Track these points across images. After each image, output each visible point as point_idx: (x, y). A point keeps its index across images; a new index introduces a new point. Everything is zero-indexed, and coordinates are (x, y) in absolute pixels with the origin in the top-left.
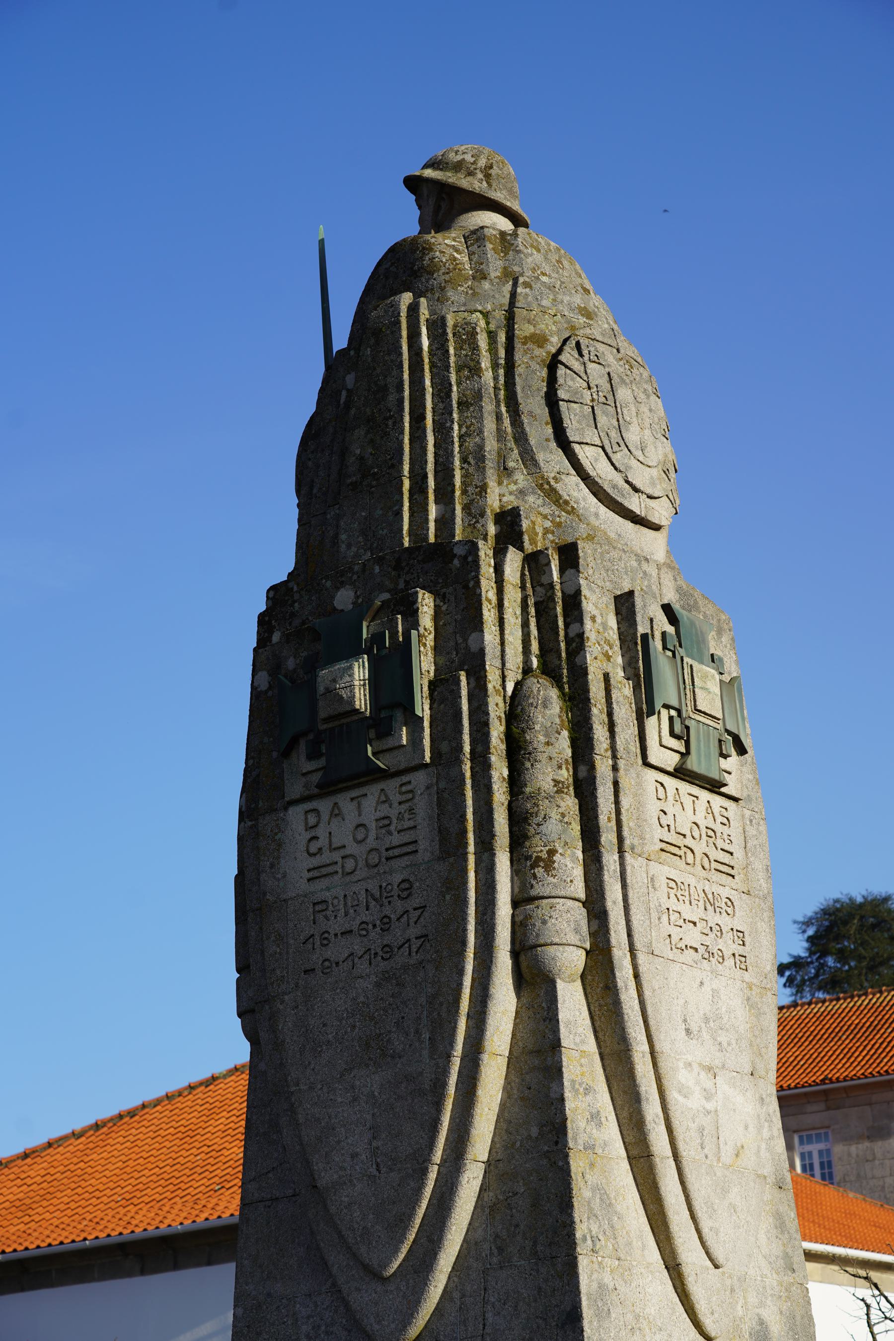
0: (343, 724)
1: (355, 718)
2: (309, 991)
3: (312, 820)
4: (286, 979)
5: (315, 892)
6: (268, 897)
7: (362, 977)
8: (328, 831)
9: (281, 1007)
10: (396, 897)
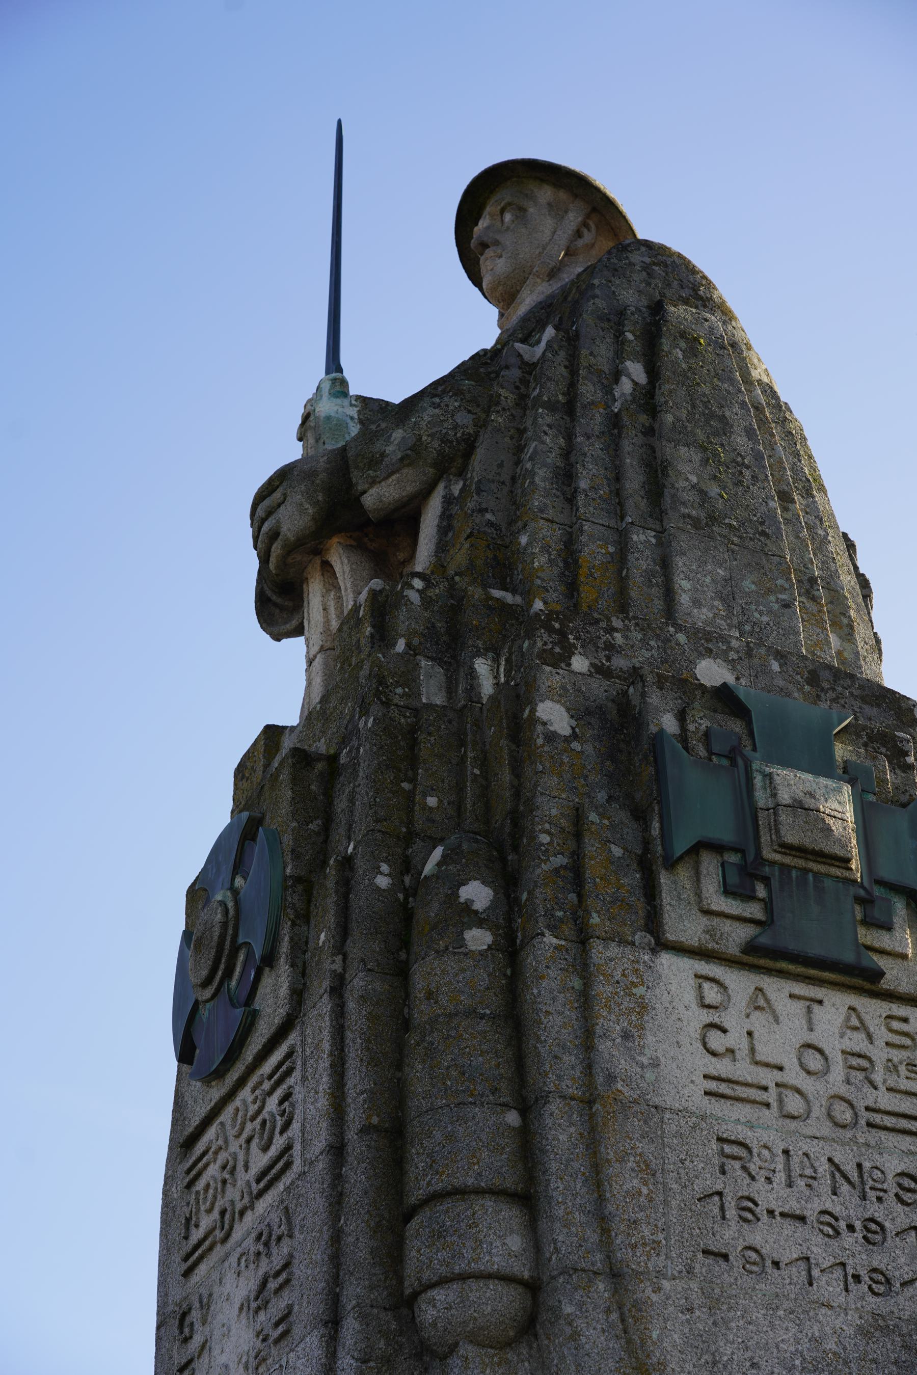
0: (811, 871)
1: (837, 872)
2: (717, 1291)
3: (712, 994)
4: (664, 1250)
5: (724, 1120)
6: (619, 1086)
7: (830, 1307)
8: (747, 1027)
9: (655, 1298)
10: (891, 1194)
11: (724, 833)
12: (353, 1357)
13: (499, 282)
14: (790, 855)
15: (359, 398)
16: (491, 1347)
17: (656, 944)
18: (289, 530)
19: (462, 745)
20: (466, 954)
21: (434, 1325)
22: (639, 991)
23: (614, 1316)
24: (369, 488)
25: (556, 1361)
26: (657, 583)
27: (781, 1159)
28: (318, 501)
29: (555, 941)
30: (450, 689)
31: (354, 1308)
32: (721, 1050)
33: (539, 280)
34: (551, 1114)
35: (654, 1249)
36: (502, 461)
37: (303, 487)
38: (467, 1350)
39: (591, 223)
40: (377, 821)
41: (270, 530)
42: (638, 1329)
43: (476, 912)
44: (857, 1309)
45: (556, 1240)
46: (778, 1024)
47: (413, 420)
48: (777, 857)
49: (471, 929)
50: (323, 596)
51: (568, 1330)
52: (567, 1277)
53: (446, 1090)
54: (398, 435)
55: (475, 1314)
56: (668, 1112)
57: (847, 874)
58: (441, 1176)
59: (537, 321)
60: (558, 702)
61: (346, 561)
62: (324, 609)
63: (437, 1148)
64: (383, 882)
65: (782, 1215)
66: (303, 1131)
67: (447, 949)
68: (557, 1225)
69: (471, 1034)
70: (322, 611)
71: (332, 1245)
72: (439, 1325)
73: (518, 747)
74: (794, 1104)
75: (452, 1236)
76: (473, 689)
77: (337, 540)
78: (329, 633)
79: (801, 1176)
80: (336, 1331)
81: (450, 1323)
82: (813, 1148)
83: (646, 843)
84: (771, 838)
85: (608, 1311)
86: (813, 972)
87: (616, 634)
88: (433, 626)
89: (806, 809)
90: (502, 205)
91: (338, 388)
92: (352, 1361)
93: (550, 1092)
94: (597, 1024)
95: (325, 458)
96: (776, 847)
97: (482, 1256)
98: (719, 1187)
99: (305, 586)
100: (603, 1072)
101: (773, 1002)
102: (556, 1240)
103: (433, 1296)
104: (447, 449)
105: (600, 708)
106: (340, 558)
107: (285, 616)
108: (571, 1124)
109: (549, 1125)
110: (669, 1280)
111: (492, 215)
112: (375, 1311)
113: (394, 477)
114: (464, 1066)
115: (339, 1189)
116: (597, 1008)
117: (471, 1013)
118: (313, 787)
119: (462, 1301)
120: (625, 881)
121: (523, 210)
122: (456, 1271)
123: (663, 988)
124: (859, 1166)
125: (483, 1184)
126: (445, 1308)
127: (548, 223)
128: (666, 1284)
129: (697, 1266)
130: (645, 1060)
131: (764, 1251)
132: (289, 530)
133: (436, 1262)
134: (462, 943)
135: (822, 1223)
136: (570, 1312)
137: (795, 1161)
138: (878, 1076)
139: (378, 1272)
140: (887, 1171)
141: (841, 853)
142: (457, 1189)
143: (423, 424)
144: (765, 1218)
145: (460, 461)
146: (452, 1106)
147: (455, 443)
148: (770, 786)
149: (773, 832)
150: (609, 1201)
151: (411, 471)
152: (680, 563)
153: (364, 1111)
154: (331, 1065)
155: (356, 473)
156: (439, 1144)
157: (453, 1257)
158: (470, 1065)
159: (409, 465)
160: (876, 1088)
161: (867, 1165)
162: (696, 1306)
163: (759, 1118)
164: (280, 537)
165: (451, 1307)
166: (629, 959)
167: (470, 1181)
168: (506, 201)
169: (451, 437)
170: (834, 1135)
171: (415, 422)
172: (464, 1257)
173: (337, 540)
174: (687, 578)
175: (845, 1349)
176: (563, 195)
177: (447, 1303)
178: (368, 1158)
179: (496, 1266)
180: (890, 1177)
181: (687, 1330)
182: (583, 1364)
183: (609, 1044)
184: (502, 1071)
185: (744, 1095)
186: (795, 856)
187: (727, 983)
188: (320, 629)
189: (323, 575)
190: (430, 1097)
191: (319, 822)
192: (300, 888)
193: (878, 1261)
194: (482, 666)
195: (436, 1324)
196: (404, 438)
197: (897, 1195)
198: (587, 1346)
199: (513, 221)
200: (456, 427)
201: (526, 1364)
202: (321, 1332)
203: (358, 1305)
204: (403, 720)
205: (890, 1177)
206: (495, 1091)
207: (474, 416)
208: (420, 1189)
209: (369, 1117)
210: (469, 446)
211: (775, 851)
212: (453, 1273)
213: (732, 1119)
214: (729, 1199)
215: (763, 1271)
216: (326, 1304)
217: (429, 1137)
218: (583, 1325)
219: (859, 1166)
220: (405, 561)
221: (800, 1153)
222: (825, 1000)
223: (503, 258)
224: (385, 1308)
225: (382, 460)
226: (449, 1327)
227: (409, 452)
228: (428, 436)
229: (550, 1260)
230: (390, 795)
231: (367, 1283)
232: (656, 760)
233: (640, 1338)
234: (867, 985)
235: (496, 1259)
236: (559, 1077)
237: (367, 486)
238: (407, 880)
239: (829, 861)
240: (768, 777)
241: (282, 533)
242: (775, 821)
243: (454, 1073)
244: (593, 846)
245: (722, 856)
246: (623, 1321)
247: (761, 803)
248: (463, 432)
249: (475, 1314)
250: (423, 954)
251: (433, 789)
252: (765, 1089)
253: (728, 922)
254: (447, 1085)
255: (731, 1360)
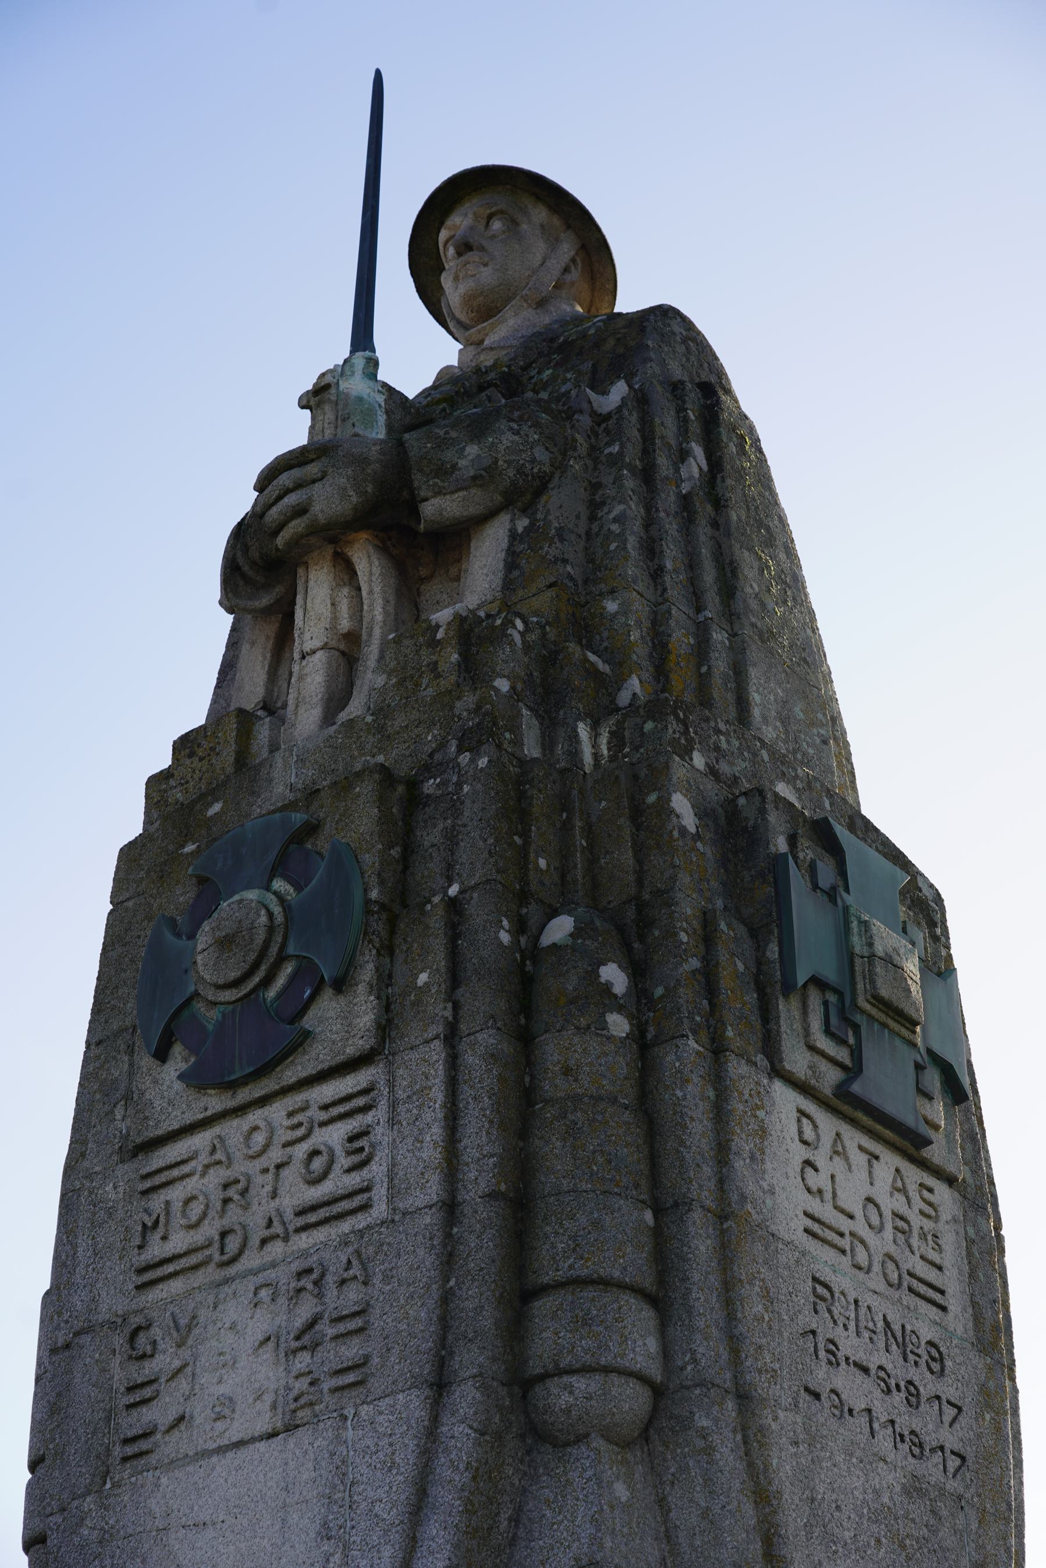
1: (904, 1032)
11: (830, 973)
12: (471, 1427)
13: (482, 292)
14: (877, 1007)
15: (385, 385)
16: (617, 1444)
17: (771, 1069)
18: (322, 511)
19: (563, 811)
20: (608, 1038)
21: (568, 1411)
22: (761, 1114)
23: (739, 1437)
24: (432, 497)
25: (672, 1470)
26: (731, 688)
27: (852, 1307)
28: (366, 491)
29: (696, 1046)
30: (548, 744)
31: (474, 1377)
32: (814, 1189)
33: (525, 305)
34: (694, 1223)
35: (772, 1376)
36: (579, 513)
37: (350, 472)
38: (598, 1442)
39: (579, 261)
40: (498, 872)
41: (298, 505)
42: (762, 1455)
43: (616, 996)
44: (902, 1467)
45: (695, 1351)
46: (850, 1171)
47: (491, 440)
48: (868, 1007)
49: (612, 1013)
50: (332, 590)
51: (700, 1443)
52: (704, 1390)
53: (592, 1175)
54: (472, 450)
55: (615, 1410)
56: (780, 1242)
57: (911, 1037)
58: (586, 1262)
59: (539, 353)
60: (686, 796)
61: (377, 563)
62: (333, 604)
63: (581, 1233)
64: (505, 937)
65: (856, 1364)
66: (391, 1176)
67: (589, 1028)
68: (698, 1337)
69: (617, 1123)
70: (329, 605)
71: (441, 1306)
72: (573, 1412)
73: (638, 830)
74: (862, 1257)
75: (598, 1326)
76: (574, 754)
77: (366, 537)
78: (335, 631)
79: (866, 1327)
80: (440, 1395)
81: (588, 1414)
82: (868, 1299)
83: (760, 962)
84: (865, 987)
85: (734, 1431)
86: (879, 1128)
87: (721, 737)
88: (531, 675)
89: (895, 966)
90: (493, 209)
91: (371, 370)
92: (470, 1432)
93: (693, 1200)
94: (733, 1140)
95: (378, 447)
96: (869, 997)
97: (627, 1352)
98: (814, 1326)
99: (301, 571)
100: (737, 1190)
101: (847, 1149)
102: (695, 1351)
103: (571, 1382)
104: (521, 482)
105: (713, 810)
106: (369, 557)
107: (249, 591)
108: (708, 1237)
109: (693, 1233)
110: (783, 1410)
111: (476, 216)
112: (495, 1384)
113: (461, 494)
114: (610, 1154)
115: (449, 1248)
116: (733, 1124)
117: (614, 1101)
118: (394, 810)
119: (604, 1394)
120: (747, 998)
121: (515, 223)
122: (602, 1363)
123: (777, 1116)
124: (903, 1327)
125: (627, 1280)
126: (584, 1397)
127: (540, 248)
128: (781, 1414)
129: (801, 1401)
130: (765, 1184)
131: (843, 1397)
132: (322, 511)
133: (579, 1349)
134: (604, 1026)
135: (878, 1377)
136: (705, 1425)
137: (863, 1311)
138: (915, 1242)
139: (499, 1344)
140: (921, 1338)
141: (914, 1016)
142: (602, 1279)
143: (501, 448)
144: (843, 1364)
145: (529, 497)
146: (598, 1192)
147: (530, 478)
148: (865, 934)
149: (867, 981)
150: (740, 1321)
151: (479, 493)
152: (754, 673)
153: (494, 1176)
154: (445, 1117)
155: (418, 476)
156: (584, 1229)
157: (599, 1347)
158: (616, 1154)
159: (481, 486)
160: (913, 1252)
161: (908, 1328)
162: (800, 1440)
163: (840, 1263)
164: (308, 515)
165: (591, 1398)
166: (754, 1079)
167: (617, 1274)
168: (499, 208)
169: (527, 471)
170: (887, 1293)
171: (493, 443)
172: (610, 1350)
173: (366, 537)
174: (757, 691)
175: (895, 1504)
176: (556, 221)
177: (587, 1393)
178: (496, 1225)
179: (639, 1366)
180: (923, 1343)
181: (794, 1463)
182: (715, 1480)
183: (742, 1163)
184: (642, 1167)
185: (830, 1238)
186: (880, 1010)
187: (818, 1122)
188: (325, 623)
189: (334, 566)
190: (573, 1178)
191: (398, 849)
192: (384, 916)
193: (916, 1425)
194: (583, 731)
195: (571, 1411)
196: (479, 456)
197: (927, 1362)
198: (721, 1463)
199: (504, 232)
200: (533, 461)
201: (640, 1467)
202: (426, 1393)
203: (481, 1375)
204: (511, 769)
205: (923, 1343)
206: (637, 1186)
207: (551, 456)
208: (557, 1270)
209: (498, 1183)
210: (542, 485)
211: (867, 1001)
212: (598, 1364)
213: (822, 1260)
214: (821, 1339)
215: (842, 1416)
216: (433, 1365)
217: (572, 1219)
218: (718, 1441)
219: (903, 1327)
220: (425, 579)
221: (866, 1304)
222: (881, 1156)
223: (490, 267)
224: (502, 1383)
225: (453, 472)
226: (585, 1417)
227: (483, 472)
228: (505, 461)
229: (682, 1369)
230: (505, 846)
231: (490, 1353)
232: (775, 882)
233: (763, 1463)
234: (912, 1150)
235: (639, 1359)
236: (701, 1187)
237: (430, 494)
238: (523, 940)
239: (903, 1021)
240: (863, 924)
241: (311, 512)
242: (869, 970)
243: (600, 1159)
244: (724, 955)
245: (824, 994)
246: (745, 1443)
247: (857, 950)
248: (540, 468)
249: (615, 1410)
250: (558, 1026)
251: (543, 851)
252: (841, 1235)
253: (824, 1061)
254: (592, 1169)
255: (823, 1499)
